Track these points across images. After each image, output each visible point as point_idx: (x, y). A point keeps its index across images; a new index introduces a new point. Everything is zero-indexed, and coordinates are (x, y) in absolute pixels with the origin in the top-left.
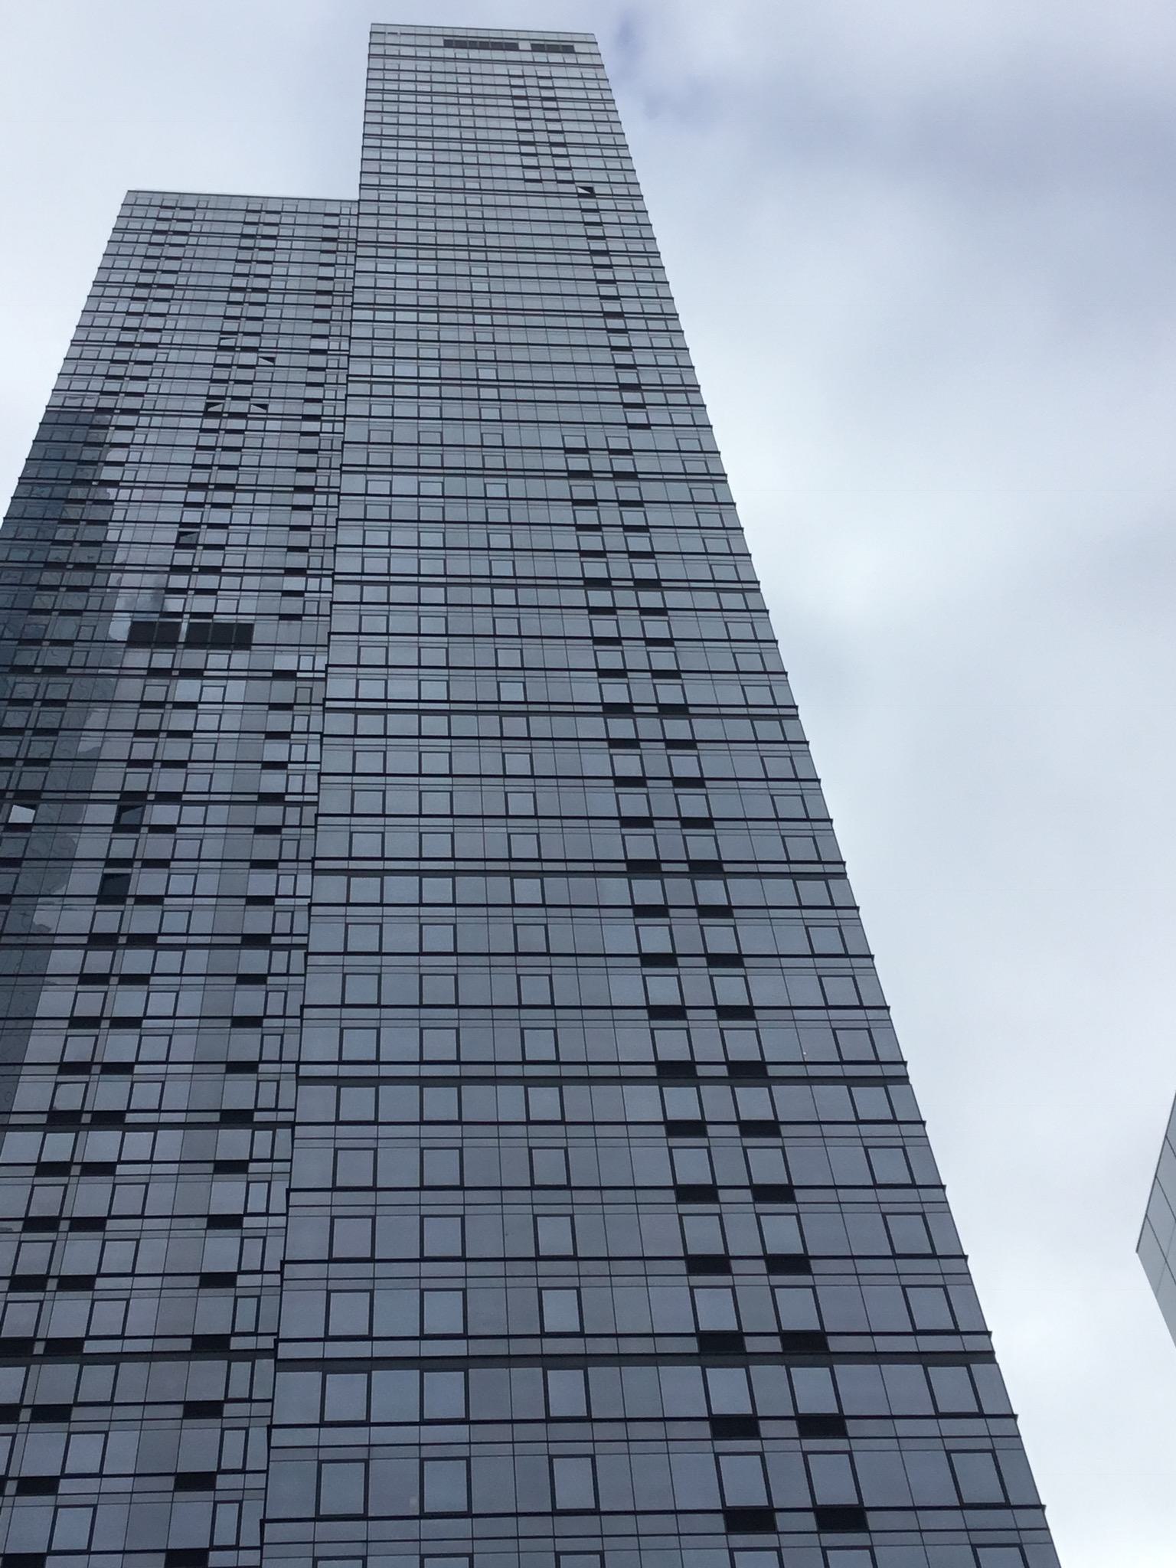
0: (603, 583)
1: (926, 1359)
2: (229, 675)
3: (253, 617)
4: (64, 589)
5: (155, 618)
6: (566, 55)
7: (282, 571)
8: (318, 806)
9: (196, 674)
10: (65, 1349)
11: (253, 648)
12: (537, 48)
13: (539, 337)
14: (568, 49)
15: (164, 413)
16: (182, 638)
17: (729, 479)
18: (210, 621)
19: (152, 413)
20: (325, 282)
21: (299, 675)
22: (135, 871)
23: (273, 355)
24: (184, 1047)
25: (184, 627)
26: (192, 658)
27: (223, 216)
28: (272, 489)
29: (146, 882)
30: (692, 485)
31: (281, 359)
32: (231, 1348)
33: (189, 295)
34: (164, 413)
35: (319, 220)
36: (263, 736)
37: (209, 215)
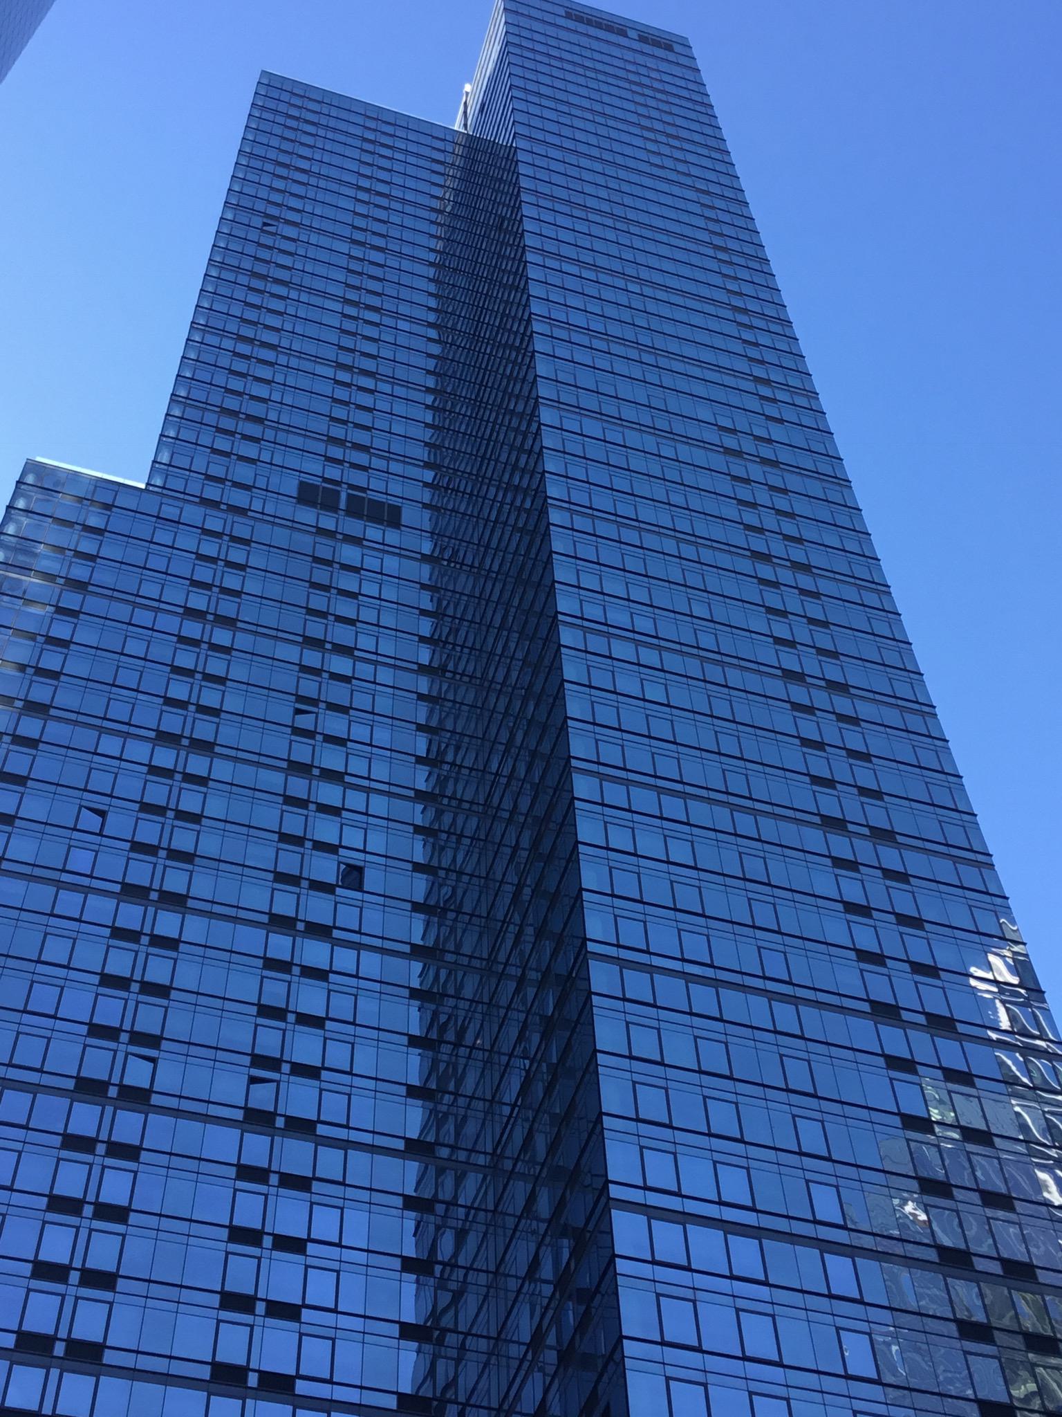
0: (766, 558)
2: (384, 548)
3: (400, 500)
5: (317, 481)
6: (667, 52)
9: (357, 541)
10: (302, 1127)
12: (643, 39)
13: (680, 315)
14: (669, 48)
15: (311, 291)
16: (343, 505)
18: (364, 495)
19: (300, 287)
21: (250, 514)
25: (343, 496)
26: (353, 526)
27: (344, 115)
28: (406, 384)
30: (563, 413)
32: (105, 1361)
34: (311, 291)
35: (428, 140)
36: (417, 612)
37: (334, 112)
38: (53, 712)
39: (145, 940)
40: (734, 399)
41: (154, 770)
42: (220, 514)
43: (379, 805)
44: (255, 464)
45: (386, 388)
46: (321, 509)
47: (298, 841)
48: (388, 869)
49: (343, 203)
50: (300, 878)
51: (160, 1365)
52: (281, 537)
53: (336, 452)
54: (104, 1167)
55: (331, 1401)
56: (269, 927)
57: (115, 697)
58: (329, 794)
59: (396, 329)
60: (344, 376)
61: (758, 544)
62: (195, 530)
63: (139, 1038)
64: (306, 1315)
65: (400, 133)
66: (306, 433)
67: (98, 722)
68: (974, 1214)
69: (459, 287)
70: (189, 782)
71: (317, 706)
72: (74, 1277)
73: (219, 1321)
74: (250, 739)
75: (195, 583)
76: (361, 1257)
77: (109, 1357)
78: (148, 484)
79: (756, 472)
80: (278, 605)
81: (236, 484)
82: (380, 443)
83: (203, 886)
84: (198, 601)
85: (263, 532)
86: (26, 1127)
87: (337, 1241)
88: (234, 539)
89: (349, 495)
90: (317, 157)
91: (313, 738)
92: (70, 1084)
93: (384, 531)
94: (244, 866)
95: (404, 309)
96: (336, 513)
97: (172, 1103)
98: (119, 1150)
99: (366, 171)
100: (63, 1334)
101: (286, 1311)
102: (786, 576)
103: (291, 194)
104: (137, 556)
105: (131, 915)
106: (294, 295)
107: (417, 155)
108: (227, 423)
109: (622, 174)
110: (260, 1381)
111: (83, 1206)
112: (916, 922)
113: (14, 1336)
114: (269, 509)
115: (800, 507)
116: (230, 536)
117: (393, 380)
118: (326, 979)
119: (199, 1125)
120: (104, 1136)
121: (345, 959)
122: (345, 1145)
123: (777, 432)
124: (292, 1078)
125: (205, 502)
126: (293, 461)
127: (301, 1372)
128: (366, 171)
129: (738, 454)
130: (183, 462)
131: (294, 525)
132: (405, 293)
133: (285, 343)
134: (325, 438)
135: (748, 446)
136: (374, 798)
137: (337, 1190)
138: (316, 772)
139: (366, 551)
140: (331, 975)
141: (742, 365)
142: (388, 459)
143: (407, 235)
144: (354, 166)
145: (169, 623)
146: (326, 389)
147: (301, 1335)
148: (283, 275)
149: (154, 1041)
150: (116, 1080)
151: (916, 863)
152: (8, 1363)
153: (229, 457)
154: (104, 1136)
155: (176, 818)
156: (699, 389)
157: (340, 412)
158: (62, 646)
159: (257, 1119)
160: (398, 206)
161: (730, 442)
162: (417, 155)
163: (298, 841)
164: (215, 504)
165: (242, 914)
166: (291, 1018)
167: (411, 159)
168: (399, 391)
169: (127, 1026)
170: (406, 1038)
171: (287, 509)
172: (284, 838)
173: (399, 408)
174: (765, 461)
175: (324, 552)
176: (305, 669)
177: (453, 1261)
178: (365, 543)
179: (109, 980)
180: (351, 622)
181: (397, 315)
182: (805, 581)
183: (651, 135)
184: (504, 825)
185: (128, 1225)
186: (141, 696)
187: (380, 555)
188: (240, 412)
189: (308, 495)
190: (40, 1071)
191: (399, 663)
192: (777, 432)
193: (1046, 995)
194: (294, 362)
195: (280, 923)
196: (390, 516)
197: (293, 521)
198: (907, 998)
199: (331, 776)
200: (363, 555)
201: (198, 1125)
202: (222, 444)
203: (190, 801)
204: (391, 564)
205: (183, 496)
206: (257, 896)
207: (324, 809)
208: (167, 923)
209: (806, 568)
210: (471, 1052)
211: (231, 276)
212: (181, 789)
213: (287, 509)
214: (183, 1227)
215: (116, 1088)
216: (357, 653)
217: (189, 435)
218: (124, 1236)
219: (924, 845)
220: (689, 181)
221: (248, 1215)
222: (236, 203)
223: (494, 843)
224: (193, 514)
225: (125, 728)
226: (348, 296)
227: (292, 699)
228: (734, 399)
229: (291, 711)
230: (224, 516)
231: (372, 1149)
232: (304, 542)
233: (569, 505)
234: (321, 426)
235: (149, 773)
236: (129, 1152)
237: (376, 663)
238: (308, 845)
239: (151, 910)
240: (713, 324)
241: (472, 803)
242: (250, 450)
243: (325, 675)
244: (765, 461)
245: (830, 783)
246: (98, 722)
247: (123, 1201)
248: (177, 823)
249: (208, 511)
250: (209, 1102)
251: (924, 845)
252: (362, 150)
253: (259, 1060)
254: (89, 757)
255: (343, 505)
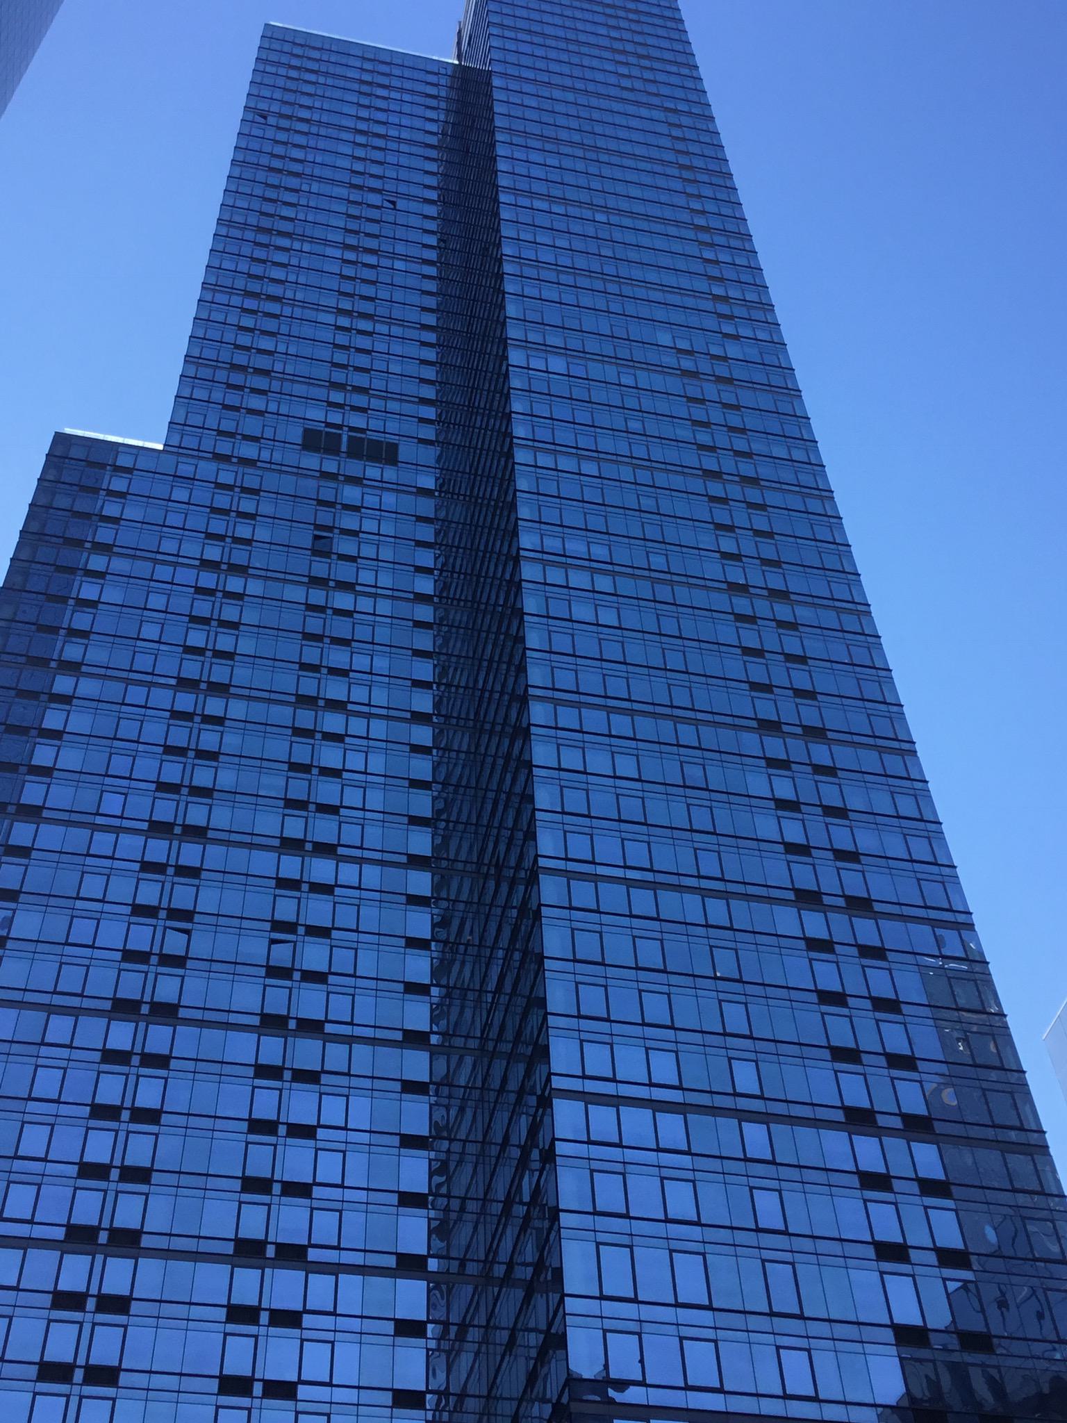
0: (716, 475)
1: (934, 923)
2: (382, 486)
3: (397, 437)
4: (239, 437)
7: (417, 400)
8: (458, 1274)
10: (311, 1027)
11: (400, 464)
15: (312, 240)
16: (344, 448)
17: (918, 747)
18: (363, 436)
19: (303, 238)
20: (430, 137)
21: (259, 464)
22: (336, 535)
23: (394, 199)
24: (375, 799)
25: (345, 438)
26: (354, 467)
28: (402, 323)
29: (346, 546)
31: (401, 204)
33: (323, 131)
35: (421, 76)
38: (84, 669)
39: (191, 754)
40: (694, 320)
41: (200, 590)
42: (231, 468)
43: (379, 729)
44: (263, 416)
45: (383, 329)
46: (324, 453)
47: (315, 668)
48: (386, 824)
49: (347, 109)
50: (308, 802)
51: (190, 1244)
52: (288, 484)
53: (337, 397)
54: (138, 1076)
55: (339, 1264)
56: (280, 850)
57: (126, 716)
58: (333, 722)
59: (393, 269)
60: (350, 256)
61: (710, 463)
62: (202, 509)
63: (174, 914)
64: (321, 1133)
65: (397, 72)
66: (309, 381)
67: (124, 675)
68: (880, 1075)
69: (454, 445)
70: (228, 598)
71: (332, 532)
72: (125, 1115)
73: (265, 986)
74: (260, 678)
75: (209, 536)
76: (365, 1138)
77: (146, 1241)
78: (165, 445)
79: (711, 391)
80: (286, 549)
81: (246, 438)
82: (378, 384)
83: (222, 817)
84: (213, 553)
85: (271, 481)
86: (145, 707)
87: (328, 1380)
88: (244, 490)
89: (349, 437)
90: (317, 104)
91: (324, 612)
92: (145, 826)
93: (382, 469)
94: (257, 796)
95: (400, 248)
96: (338, 455)
97: (198, 1015)
98: (168, 960)
99: (364, 113)
100: (147, 998)
101: (298, 1190)
102: (734, 491)
103: (286, 189)
104: (156, 515)
105: (158, 850)
106: (297, 245)
107: (412, 92)
108: (250, 304)
109: (594, 102)
110: (298, 1025)
111: (98, 1233)
112: (841, 812)
113: (111, 1002)
114: (289, 370)
115: (751, 421)
116: (218, 620)
117: (390, 321)
118: (347, 676)
119: (246, 851)
120: (164, 904)
121: (348, 873)
122: (350, 1040)
123: (733, 350)
124: (311, 895)
125: (218, 457)
126: (298, 410)
127: (321, 1123)
128: (364, 113)
129: (695, 374)
130: (196, 420)
131: (299, 472)
132: (400, 233)
133: (289, 294)
134: (327, 384)
135: (704, 366)
136: (375, 723)
137: (343, 1081)
138: (321, 703)
139: (366, 490)
140: (341, 810)
141: (701, 285)
142: (389, 324)
143: (403, 175)
144: (352, 110)
145: (186, 576)
146: (328, 335)
147: (312, 1209)
148: (287, 227)
149: (188, 915)
150: (179, 821)
151: (844, 757)
152: (59, 1253)
153: (239, 411)
154: (156, 950)
155: (214, 656)
156: (660, 314)
157: (340, 357)
158: (81, 637)
159: (272, 1023)
160: (394, 146)
161: (687, 364)
162: (412, 92)
163: (315, 668)
164: (225, 458)
165: (256, 840)
166: (312, 807)
167: (407, 97)
168: (396, 330)
169: (172, 862)
170: (404, 897)
171: (292, 457)
172: (304, 666)
173: (397, 348)
174: (719, 379)
175: (327, 495)
176: (311, 607)
177: (437, 494)
178: (365, 482)
179: (163, 787)
180: (352, 559)
181: (394, 256)
182: (754, 495)
183: (622, 58)
184: (504, 1063)
185: (118, 1387)
186: (163, 647)
187: (379, 492)
188: (232, 456)
189: (314, 441)
190: (81, 995)
191: (400, 488)
192: (733, 350)
193: (1047, 1135)
194: (298, 312)
195: (290, 845)
196: (386, 453)
197: (298, 468)
198: (829, 883)
199: (336, 706)
200: (363, 494)
201: (189, 1265)
202: (233, 398)
203: (209, 740)
204: (389, 500)
205: (197, 454)
206: (268, 823)
207: (330, 737)
208: (214, 706)
209: (754, 481)
210: (464, 1147)
211: (238, 233)
212: (187, 803)
213: (292, 457)
214: (208, 1123)
215: (139, 1057)
216: (358, 588)
217: (200, 394)
218: (157, 1135)
219: (851, 740)
220: (655, 101)
221: (265, 1108)
222: (255, 115)
223: (480, 755)
224: (207, 469)
225: (149, 678)
226: (358, 128)
227: (312, 527)
228: (694, 320)
229: (310, 538)
230: (235, 468)
231: (382, 863)
232: (309, 486)
233: (514, 190)
234: (322, 372)
235: (172, 717)
236: (161, 1061)
237: (375, 596)
238: (315, 771)
239: (175, 843)
240: (677, 247)
241: (466, 862)
242: (256, 402)
243: (329, 612)
244: (719, 379)
245: (767, 688)
246: (124, 675)
247: (155, 1105)
248: (214, 660)
249: (221, 466)
250: (229, 1011)
251: (851, 740)
252: (360, 93)
253: (278, 926)
254: (146, 583)
255: (344, 448)
